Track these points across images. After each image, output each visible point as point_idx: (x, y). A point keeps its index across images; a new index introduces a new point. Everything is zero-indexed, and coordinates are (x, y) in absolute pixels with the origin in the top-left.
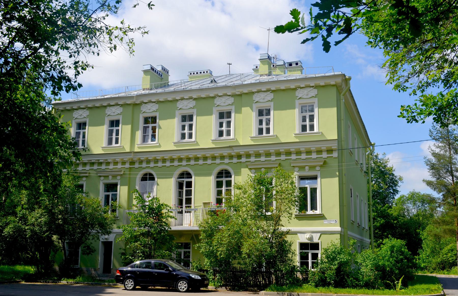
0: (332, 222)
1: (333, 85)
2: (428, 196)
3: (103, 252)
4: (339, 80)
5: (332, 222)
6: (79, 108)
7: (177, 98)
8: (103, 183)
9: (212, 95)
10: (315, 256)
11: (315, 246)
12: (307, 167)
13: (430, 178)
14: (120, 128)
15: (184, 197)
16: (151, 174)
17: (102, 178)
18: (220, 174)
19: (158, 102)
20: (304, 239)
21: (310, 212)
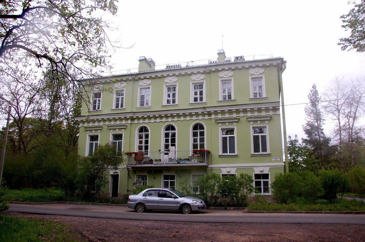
0: (278, 160)
1: (275, 66)
2: (137, 194)
3: (112, 182)
4: (280, 62)
5: (278, 160)
6: (223, 70)
7: (165, 75)
8: (89, 136)
9: (189, 73)
10: (266, 184)
11: (266, 176)
12: (259, 121)
13: (307, 136)
14: (101, 99)
15: (198, 138)
16: (145, 127)
17: (88, 132)
18: (195, 127)
19: (180, 75)
20: (257, 172)
21: (261, 153)
